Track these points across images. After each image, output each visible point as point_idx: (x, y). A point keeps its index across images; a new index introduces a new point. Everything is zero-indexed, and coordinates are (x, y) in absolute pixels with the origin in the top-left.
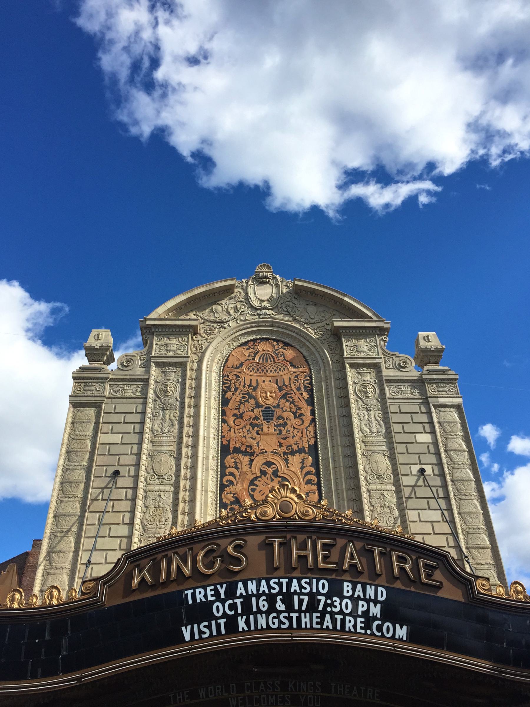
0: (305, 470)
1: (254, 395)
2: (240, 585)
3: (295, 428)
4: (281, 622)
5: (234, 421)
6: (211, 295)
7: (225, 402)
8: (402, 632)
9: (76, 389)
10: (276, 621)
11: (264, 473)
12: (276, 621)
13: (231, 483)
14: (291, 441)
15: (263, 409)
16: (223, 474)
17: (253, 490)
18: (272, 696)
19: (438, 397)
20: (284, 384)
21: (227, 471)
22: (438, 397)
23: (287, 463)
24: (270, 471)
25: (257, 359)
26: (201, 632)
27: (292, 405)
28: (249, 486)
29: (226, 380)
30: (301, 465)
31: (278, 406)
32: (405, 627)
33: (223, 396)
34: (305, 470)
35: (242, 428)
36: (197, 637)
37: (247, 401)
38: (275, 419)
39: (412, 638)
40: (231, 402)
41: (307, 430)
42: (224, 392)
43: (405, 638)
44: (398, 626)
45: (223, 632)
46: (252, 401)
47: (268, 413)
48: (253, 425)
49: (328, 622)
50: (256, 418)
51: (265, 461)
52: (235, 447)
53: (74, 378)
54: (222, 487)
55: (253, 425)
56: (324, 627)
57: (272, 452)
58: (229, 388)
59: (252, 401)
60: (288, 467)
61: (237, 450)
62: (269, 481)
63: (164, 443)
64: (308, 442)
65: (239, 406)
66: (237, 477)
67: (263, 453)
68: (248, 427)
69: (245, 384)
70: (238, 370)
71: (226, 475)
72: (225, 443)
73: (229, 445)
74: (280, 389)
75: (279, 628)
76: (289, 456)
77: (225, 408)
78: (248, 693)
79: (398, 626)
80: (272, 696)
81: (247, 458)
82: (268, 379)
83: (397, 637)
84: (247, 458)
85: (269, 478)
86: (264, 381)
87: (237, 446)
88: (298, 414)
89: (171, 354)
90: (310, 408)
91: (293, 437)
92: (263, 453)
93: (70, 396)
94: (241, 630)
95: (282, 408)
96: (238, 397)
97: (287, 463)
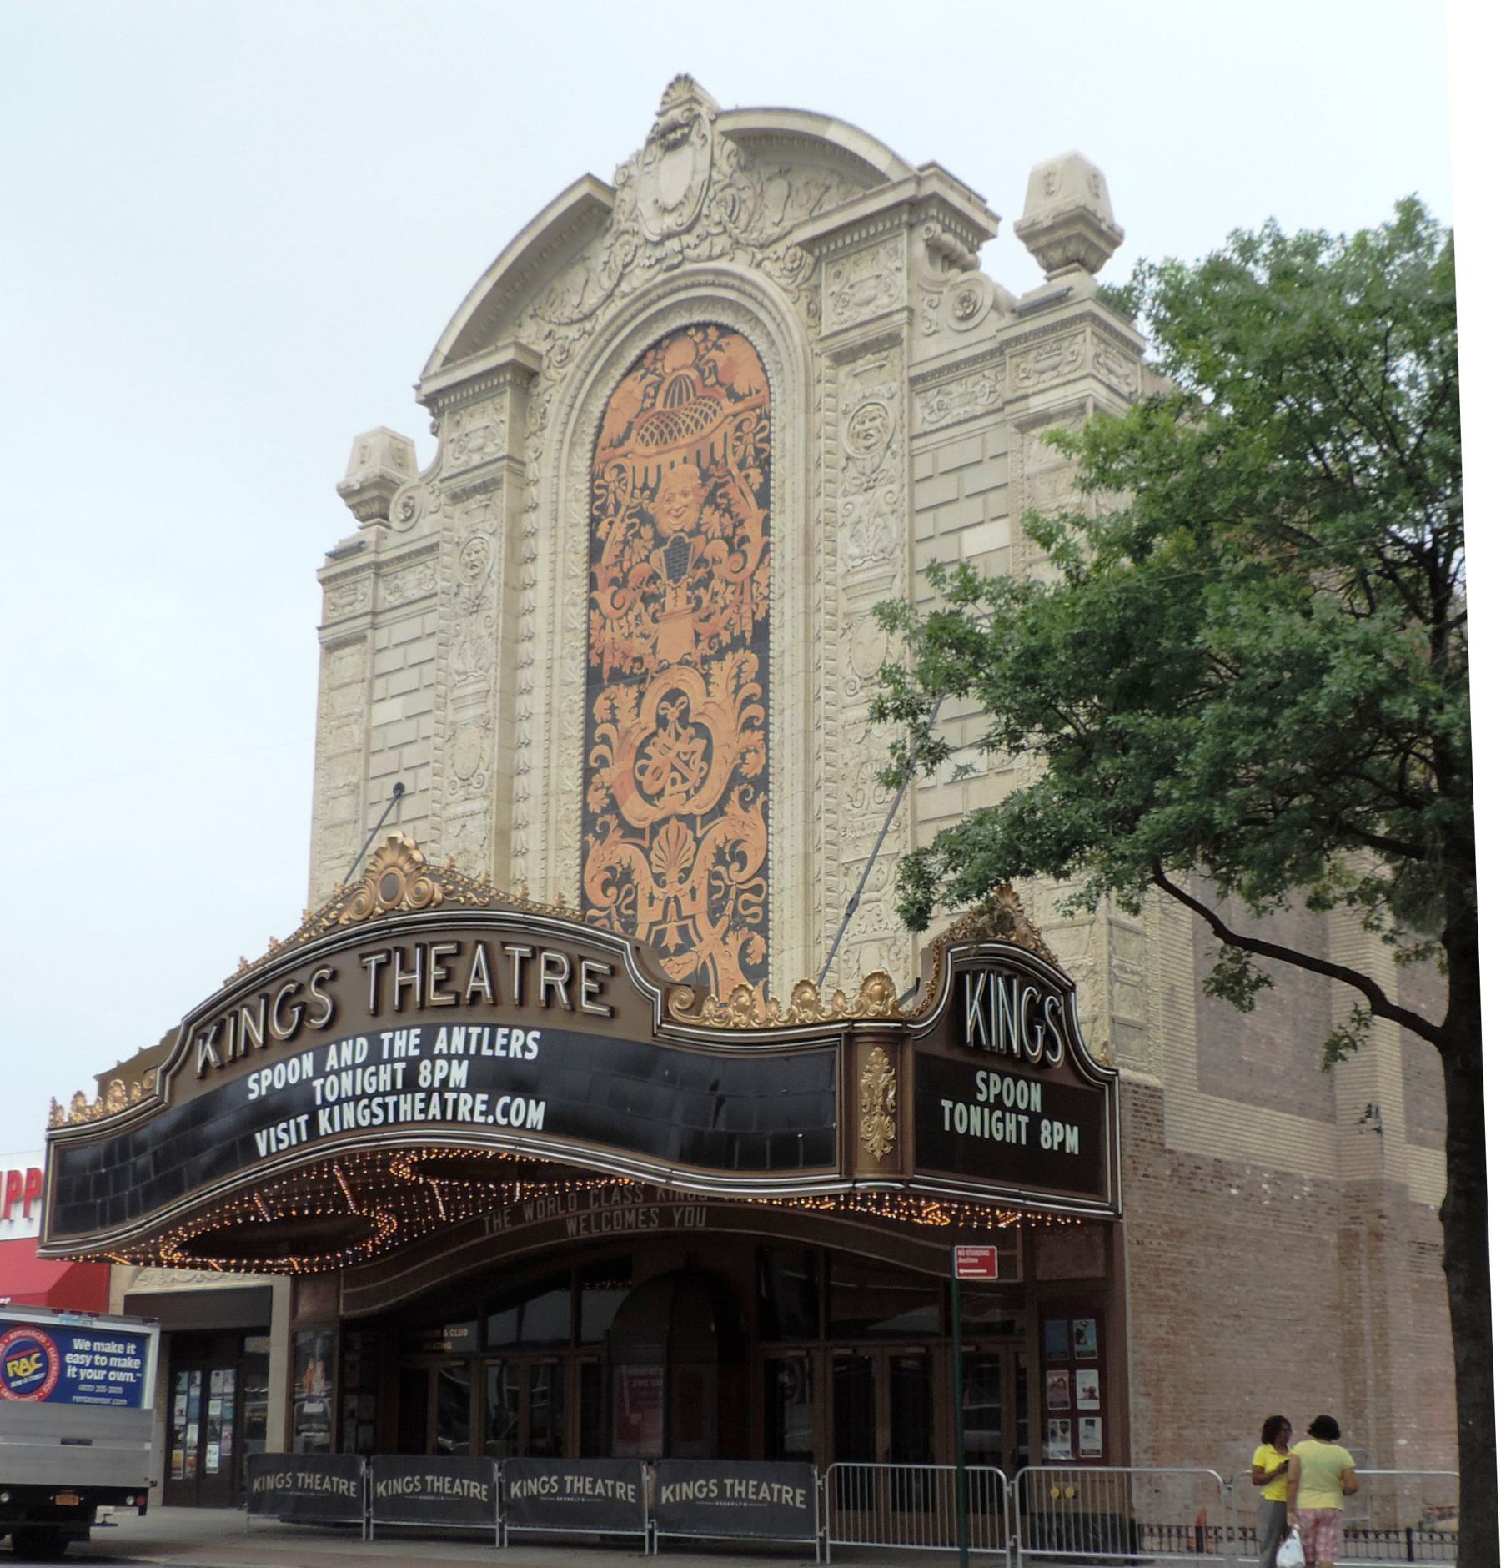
0: (743, 694)
1: (651, 512)
2: (443, 1031)
3: (728, 584)
4: (373, 1115)
5: (614, 595)
6: (554, 245)
7: (595, 550)
8: (536, 1114)
9: (329, 605)
10: (367, 1112)
11: (662, 722)
12: (367, 1112)
13: (603, 761)
14: (719, 621)
15: (667, 547)
16: (588, 744)
17: (642, 770)
18: (630, 1210)
19: (1026, 397)
20: (713, 461)
21: (598, 733)
22: (1026, 397)
23: (708, 683)
24: (673, 713)
25: (659, 407)
26: (279, 1141)
27: (727, 519)
28: (636, 760)
29: (599, 487)
30: (734, 682)
31: (696, 531)
32: (542, 1104)
33: (592, 534)
34: (743, 694)
35: (626, 614)
36: (274, 1150)
37: (637, 535)
38: (689, 567)
39: (555, 1124)
40: (608, 545)
41: (753, 581)
42: (594, 522)
43: (540, 1127)
44: (532, 1103)
45: (304, 1138)
46: (647, 532)
47: (678, 556)
48: (646, 599)
49: (434, 1110)
50: (654, 578)
51: (665, 690)
52: (612, 669)
53: (323, 582)
54: (588, 773)
55: (646, 599)
56: (430, 1117)
57: (680, 663)
58: (603, 508)
59: (647, 532)
60: (708, 694)
61: (617, 676)
62: (670, 742)
63: (470, 701)
64: (754, 613)
65: (622, 551)
66: (615, 745)
67: (664, 669)
68: (640, 605)
69: (634, 487)
70: (620, 450)
71: (596, 744)
72: (595, 662)
73: (601, 666)
74: (705, 476)
75: (371, 1125)
76: (714, 664)
77: (595, 569)
78: (594, 1208)
79: (532, 1103)
80: (630, 1210)
81: (633, 692)
82: (678, 460)
83: (528, 1126)
84: (633, 692)
85: (673, 735)
86: (672, 465)
87: (616, 665)
88: (736, 540)
89: (476, 459)
90: (762, 513)
91: (723, 609)
92: (664, 669)
93: (320, 629)
94: (322, 1133)
95: (706, 533)
96: (619, 531)
97: (708, 683)
